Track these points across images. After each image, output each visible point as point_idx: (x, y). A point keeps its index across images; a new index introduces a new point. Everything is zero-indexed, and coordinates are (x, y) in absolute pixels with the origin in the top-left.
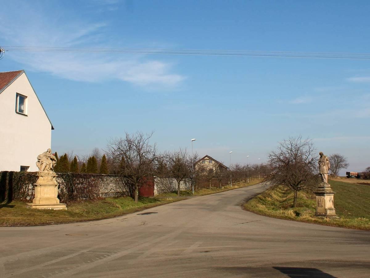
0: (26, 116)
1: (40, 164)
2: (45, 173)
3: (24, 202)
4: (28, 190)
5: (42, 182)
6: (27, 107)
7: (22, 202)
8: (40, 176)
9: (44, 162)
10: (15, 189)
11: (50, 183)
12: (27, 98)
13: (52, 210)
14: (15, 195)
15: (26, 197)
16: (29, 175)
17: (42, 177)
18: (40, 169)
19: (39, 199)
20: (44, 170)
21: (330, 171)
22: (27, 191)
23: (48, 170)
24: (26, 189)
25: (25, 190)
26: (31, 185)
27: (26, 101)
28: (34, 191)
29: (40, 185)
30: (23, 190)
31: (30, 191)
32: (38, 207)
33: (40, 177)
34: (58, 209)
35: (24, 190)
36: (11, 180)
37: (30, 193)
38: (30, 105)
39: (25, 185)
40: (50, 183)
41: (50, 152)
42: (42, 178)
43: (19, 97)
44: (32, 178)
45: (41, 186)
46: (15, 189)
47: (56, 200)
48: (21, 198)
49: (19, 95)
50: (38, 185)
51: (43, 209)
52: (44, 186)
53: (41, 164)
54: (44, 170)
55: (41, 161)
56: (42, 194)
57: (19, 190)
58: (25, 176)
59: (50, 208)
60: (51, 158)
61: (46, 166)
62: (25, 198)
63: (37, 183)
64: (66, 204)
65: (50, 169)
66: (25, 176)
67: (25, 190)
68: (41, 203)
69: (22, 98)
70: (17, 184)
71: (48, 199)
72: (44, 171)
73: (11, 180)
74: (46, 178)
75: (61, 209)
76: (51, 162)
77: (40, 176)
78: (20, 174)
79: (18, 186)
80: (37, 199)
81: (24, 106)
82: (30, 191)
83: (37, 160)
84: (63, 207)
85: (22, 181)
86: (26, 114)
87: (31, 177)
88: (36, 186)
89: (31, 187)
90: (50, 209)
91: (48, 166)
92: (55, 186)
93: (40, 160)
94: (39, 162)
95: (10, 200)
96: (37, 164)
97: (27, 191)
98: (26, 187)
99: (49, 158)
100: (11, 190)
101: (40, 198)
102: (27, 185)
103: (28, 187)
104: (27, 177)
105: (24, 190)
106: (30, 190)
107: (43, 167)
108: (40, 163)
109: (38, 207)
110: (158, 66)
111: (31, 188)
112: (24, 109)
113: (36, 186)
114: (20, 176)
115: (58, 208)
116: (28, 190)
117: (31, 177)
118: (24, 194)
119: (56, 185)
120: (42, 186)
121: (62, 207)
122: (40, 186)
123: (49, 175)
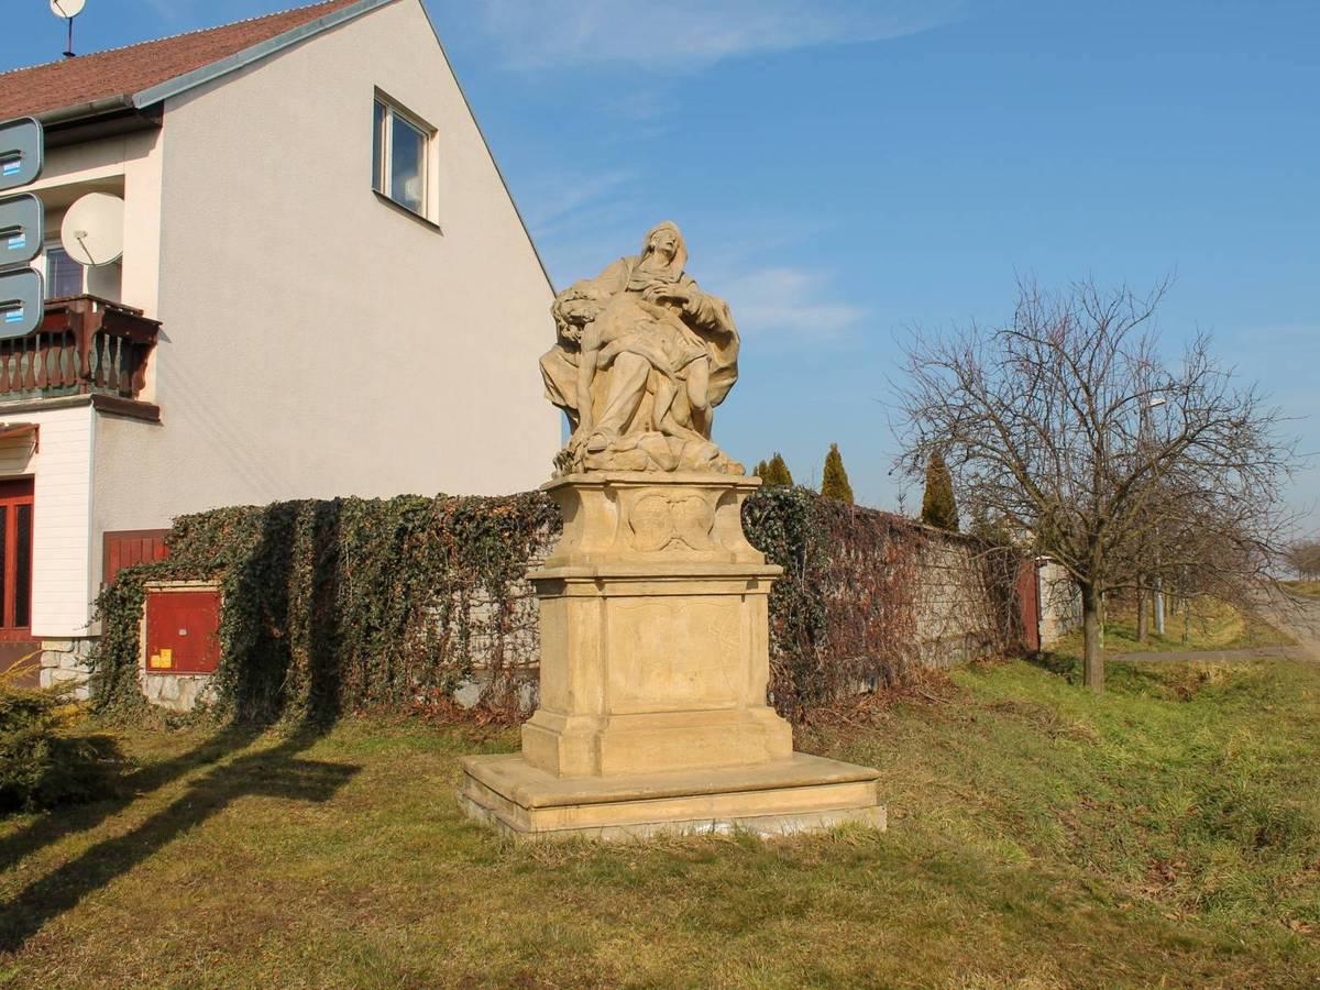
0: (435, 228)
1: (585, 371)
2: (638, 457)
3: (439, 721)
4: (465, 635)
5: (606, 545)
6: (433, 185)
7: (419, 727)
8: (592, 486)
10: (370, 629)
11: (696, 556)
12: (438, 135)
13: (745, 845)
14: (368, 672)
15: (452, 685)
16: (471, 519)
19: (593, 725)
20: (624, 429)
21: (243, 637)
22: (454, 637)
24: (445, 625)
25: (439, 630)
26: (483, 594)
27: (432, 152)
28: (508, 638)
29: (599, 581)
30: (423, 636)
31: (480, 640)
33: (584, 495)
34: (803, 827)
35: (431, 633)
36: (327, 562)
37: (480, 658)
38: (453, 168)
39: (438, 592)
40: (696, 556)
41: (671, 257)
42: (609, 505)
43: (389, 120)
44: (489, 541)
45: (608, 589)
46: (370, 629)
47: (762, 729)
48: (414, 691)
49: (390, 110)
50: (579, 580)
51: (647, 834)
52: (635, 588)
54: (624, 429)
55: (589, 336)
56: (616, 676)
57: (400, 631)
58: (439, 531)
59: (716, 819)
60: (692, 307)
61: (644, 388)
62: (448, 694)
63: (563, 562)
64: (872, 771)
65: (682, 412)
66: (439, 531)
67: (439, 630)
68: (621, 767)
69: (407, 136)
70: (380, 588)
71: (684, 720)
72: (630, 441)
73: (327, 562)
74: (647, 503)
75: (832, 821)
76: (691, 350)
77: (592, 486)
78: (403, 514)
79: (387, 605)
80: (571, 722)
82: (480, 640)
84: (834, 802)
85: (418, 564)
86: (430, 219)
87: (487, 532)
88: (552, 587)
89: (483, 611)
90: (724, 829)
91: (665, 388)
92: (741, 586)
93: (579, 322)
94: (571, 346)
95: (325, 710)
96: (552, 370)
97: (454, 637)
98: (449, 607)
99: (671, 313)
100: (327, 636)
101: (605, 717)
102: (457, 596)
103: (466, 608)
104: (453, 531)
105: (431, 633)
106: (481, 628)
108: (586, 358)
109: (588, 817)
111: (484, 617)
112: (421, 195)
113: (552, 587)
114: (402, 532)
115: (802, 813)
116: (465, 635)
117: (487, 532)
118: (436, 662)
119: (753, 580)
120: (622, 588)
121: (832, 808)
122: (592, 588)
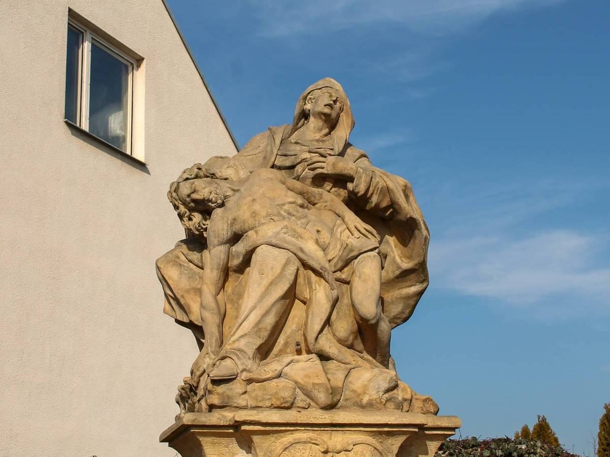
0: (141, 166)
1: (211, 274)
2: (282, 389)
8: (216, 431)
9: (269, 231)
12: (144, 65)
17: (246, 442)
18: (211, 330)
20: (264, 352)
23: (327, 344)
27: (139, 84)
32: (319, 429)
41: (331, 123)
43: (87, 47)
49: (88, 36)
53: (226, 272)
55: (218, 226)
65: (344, 326)
72: (273, 366)
76: (355, 241)
77: (216, 431)
81: (125, 116)
83: (177, 230)
96: (172, 274)
99: (331, 196)
107: (248, 301)
108: (215, 255)
110: (566, 243)
123: (340, 416)
